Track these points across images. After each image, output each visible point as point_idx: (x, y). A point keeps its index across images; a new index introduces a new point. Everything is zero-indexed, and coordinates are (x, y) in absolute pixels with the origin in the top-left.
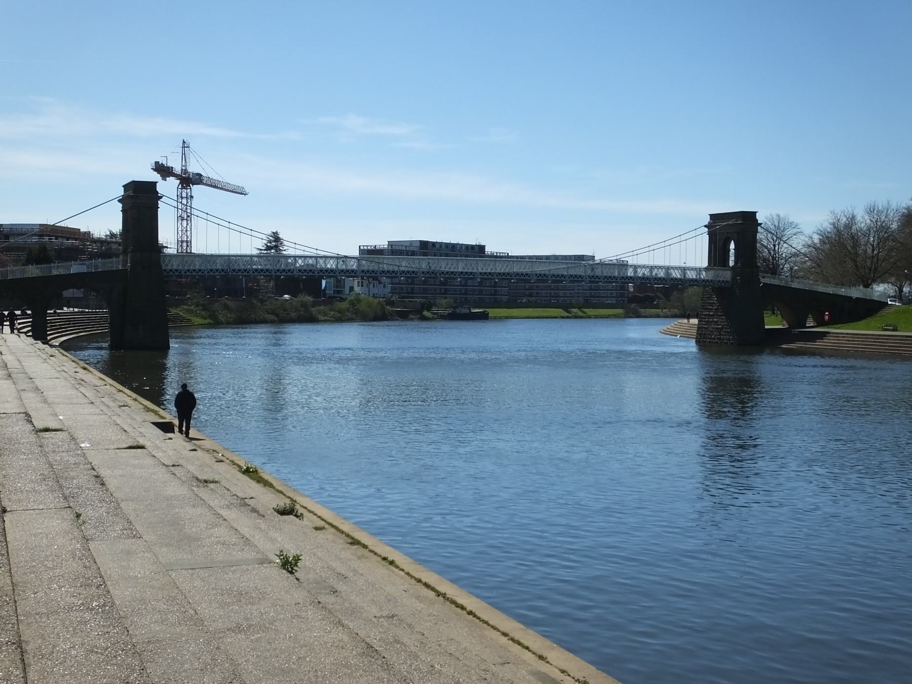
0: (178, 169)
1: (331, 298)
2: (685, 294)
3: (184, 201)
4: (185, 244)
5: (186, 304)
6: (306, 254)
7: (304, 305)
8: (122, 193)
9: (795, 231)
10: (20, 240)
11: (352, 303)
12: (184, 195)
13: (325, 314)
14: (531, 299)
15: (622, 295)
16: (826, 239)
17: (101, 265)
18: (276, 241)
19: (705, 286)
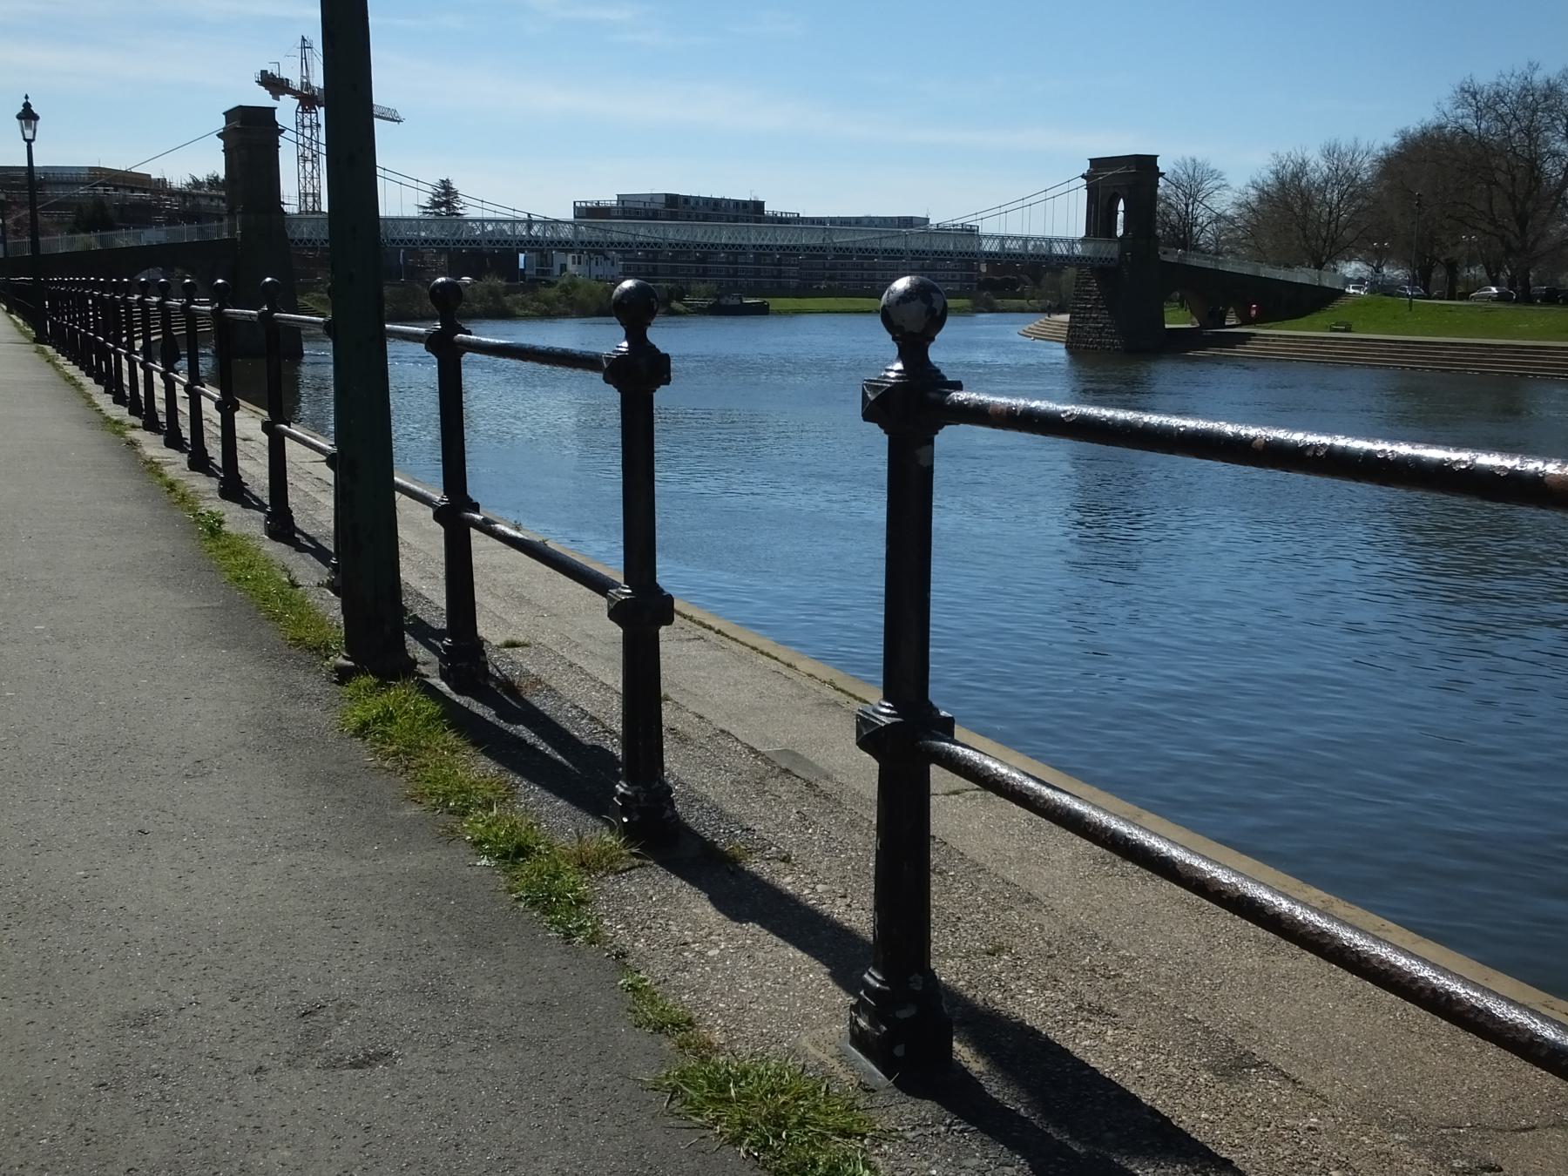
0: (296, 83)
1: (533, 281)
2: (1063, 277)
3: (308, 133)
4: (310, 199)
5: (316, 291)
6: (498, 216)
7: (492, 292)
8: (223, 124)
9: (1217, 183)
10: (61, 192)
11: (565, 290)
12: (307, 122)
13: (525, 306)
14: (832, 284)
15: (970, 278)
16: (1265, 196)
17: (187, 233)
18: (446, 195)
19: (1079, 266)
